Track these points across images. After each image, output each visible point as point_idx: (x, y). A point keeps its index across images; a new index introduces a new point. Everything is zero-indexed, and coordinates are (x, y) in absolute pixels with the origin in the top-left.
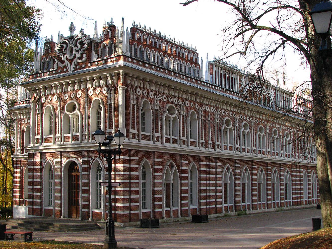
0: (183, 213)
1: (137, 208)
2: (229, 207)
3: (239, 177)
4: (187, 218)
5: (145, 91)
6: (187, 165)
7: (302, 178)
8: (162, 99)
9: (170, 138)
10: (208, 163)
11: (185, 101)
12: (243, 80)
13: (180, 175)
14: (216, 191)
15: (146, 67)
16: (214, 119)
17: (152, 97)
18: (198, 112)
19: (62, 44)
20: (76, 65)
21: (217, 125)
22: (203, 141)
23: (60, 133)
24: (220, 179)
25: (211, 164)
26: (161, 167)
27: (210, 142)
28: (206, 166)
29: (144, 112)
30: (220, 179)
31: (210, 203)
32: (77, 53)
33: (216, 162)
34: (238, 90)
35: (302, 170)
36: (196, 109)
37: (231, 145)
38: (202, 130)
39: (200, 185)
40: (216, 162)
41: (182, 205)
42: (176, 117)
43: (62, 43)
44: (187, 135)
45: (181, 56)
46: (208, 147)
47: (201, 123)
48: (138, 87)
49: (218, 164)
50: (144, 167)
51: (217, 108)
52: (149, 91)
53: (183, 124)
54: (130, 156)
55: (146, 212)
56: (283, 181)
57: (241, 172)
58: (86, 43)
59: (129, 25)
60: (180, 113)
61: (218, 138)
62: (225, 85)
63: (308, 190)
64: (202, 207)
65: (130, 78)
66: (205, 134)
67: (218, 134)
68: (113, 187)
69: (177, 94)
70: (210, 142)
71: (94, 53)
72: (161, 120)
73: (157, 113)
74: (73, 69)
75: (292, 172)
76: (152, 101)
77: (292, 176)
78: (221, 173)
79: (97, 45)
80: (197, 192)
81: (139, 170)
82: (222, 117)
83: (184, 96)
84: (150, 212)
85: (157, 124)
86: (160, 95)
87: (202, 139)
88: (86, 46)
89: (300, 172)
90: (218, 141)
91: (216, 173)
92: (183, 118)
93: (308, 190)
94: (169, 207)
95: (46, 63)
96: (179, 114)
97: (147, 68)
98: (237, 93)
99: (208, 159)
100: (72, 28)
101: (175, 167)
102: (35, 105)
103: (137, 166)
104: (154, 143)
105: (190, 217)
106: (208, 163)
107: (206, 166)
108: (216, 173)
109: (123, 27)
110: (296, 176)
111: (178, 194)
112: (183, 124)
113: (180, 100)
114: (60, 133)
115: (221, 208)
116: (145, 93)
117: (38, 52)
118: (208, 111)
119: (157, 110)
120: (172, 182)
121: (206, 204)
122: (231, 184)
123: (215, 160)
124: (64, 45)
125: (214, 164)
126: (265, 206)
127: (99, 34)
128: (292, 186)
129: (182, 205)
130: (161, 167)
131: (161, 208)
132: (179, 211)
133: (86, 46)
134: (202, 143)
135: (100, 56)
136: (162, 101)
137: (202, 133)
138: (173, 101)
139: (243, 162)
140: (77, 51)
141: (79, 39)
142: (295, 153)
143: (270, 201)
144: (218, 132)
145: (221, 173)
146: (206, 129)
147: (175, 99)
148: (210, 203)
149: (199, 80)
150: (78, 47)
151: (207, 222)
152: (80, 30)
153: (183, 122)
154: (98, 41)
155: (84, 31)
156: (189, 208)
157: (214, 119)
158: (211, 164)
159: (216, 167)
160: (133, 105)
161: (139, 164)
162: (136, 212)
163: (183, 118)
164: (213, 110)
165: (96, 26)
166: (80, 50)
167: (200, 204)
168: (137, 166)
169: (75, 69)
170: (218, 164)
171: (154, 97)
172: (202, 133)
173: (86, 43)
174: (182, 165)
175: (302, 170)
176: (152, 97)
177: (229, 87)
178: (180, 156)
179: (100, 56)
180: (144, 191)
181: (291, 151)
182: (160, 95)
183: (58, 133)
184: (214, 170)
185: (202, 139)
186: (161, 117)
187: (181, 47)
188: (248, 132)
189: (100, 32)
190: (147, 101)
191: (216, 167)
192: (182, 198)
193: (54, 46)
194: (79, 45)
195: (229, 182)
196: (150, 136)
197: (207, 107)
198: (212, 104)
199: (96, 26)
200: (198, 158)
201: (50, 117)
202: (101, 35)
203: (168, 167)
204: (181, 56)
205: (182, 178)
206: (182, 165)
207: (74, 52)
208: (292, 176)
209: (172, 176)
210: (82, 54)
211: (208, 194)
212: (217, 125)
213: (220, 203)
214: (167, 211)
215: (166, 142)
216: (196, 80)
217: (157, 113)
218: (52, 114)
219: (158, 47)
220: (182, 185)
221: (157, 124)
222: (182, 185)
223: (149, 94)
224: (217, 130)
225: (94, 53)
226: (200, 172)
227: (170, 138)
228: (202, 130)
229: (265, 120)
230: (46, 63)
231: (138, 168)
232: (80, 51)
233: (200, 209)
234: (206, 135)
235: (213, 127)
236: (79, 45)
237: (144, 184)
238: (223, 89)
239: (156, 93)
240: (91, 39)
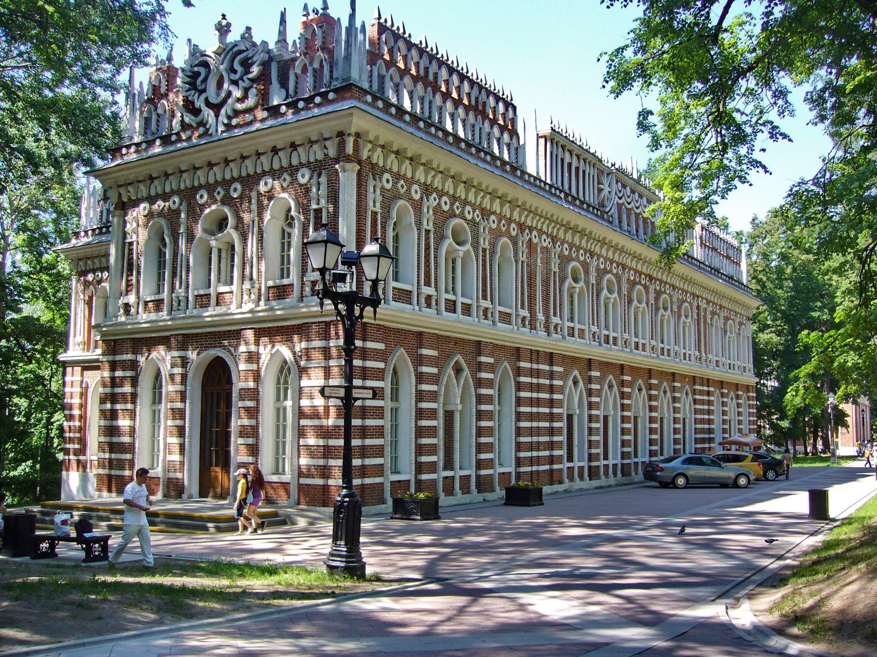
0: (484, 484)
1: (379, 470)
2: (576, 470)
3: (598, 400)
4: (489, 496)
5: (402, 182)
6: (491, 368)
7: (712, 408)
8: (439, 204)
9: (455, 302)
10: (535, 366)
11: (489, 216)
12: (605, 180)
13: (476, 391)
14: (552, 431)
15: (405, 121)
16: (547, 263)
17: (417, 197)
18: (515, 244)
19: (196, 69)
20: (229, 118)
21: (555, 277)
22: (525, 313)
23: (183, 287)
24: (560, 404)
25: (542, 367)
26: (434, 370)
27: (541, 317)
28: (532, 373)
29: (397, 235)
30: (560, 404)
31: (538, 461)
32: (232, 88)
33: (551, 365)
34: (596, 202)
35: (712, 389)
36: (511, 238)
37: (583, 327)
38: (522, 287)
39: (519, 416)
40: (551, 364)
41: (480, 464)
42: (468, 251)
43: (196, 65)
44: (491, 296)
45: (480, 108)
46: (535, 328)
47: (522, 272)
48: (384, 170)
49: (556, 368)
50: (395, 371)
51: (554, 239)
52: (410, 182)
53: (484, 270)
54: (551, 365)
55: (399, 482)
56: (679, 413)
57: (602, 389)
58: (258, 63)
59: (366, 16)
60: (478, 243)
61: (555, 308)
62: (570, 188)
63: (723, 433)
64: (523, 469)
65: (369, 146)
66: (530, 297)
67: (555, 301)
68: (356, 399)
69: (471, 197)
70: (541, 317)
71: (275, 85)
72: (436, 257)
73: (427, 239)
74: (221, 128)
75: (694, 392)
76: (418, 207)
77: (695, 401)
78: (561, 390)
79: (285, 67)
80: (511, 434)
81: (386, 375)
82: (565, 260)
83: (486, 203)
84: (409, 481)
85: (427, 266)
86: (434, 195)
87: (523, 307)
88: (255, 70)
89: (708, 393)
90: (555, 315)
91: (551, 389)
92: (484, 256)
93: (723, 433)
94: (452, 469)
95: (154, 117)
96: (475, 245)
97: (408, 123)
98: (594, 208)
99: (535, 355)
100: (223, 29)
101: (466, 372)
102: (121, 222)
103: (381, 365)
104: (420, 310)
105: (500, 493)
106: (535, 366)
107: (532, 373)
108: (551, 389)
109: (352, 17)
110: (702, 402)
111: (470, 437)
112: (484, 270)
113: (477, 212)
114: (183, 287)
115: (561, 470)
116: (402, 187)
117: (134, 94)
118: (536, 244)
119: (428, 232)
120: (460, 407)
121: (532, 461)
122: (580, 417)
123: (551, 358)
124: (202, 70)
125: (547, 368)
126: (469, 487)
127: (290, 41)
128: (695, 423)
129: (480, 464)
130: (434, 370)
131: (434, 471)
132: (513, 474)
133: (255, 70)
134: (524, 318)
135: (291, 92)
136: (437, 209)
137: (523, 294)
138: (463, 212)
139: (606, 366)
140: (235, 83)
141: (241, 52)
142: (699, 351)
143: (656, 455)
144: (555, 294)
145: (561, 390)
146: (531, 285)
147: (468, 208)
148: (538, 461)
149: (516, 169)
150: (235, 72)
151: (542, 504)
152: (243, 30)
153: (484, 266)
154: (287, 57)
155: (254, 33)
156: (495, 472)
157: (547, 263)
158: (542, 367)
159: (551, 375)
160: (375, 214)
161: (385, 361)
162: (378, 480)
163: (484, 256)
164: (546, 243)
165: (283, 21)
166: (241, 79)
167: (519, 462)
168: (381, 365)
169: (229, 127)
170: (556, 368)
171: (422, 198)
172: (523, 294)
173: (258, 63)
174: (480, 367)
175: (712, 389)
176: (417, 197)
177: (578, 193)
178: (478, 347)
179: (291, 92)
180: (395, 427)
181: (693, 348)
182: (434, 195)
183: (180, 288)
184: (547, 382)
185: (523, 307)
186: (436, 249)
187: (481, 87)
188: (615, 298)
189: (294, 33)
190: (406, 207)
191: (551, 375)
192: (480, 448)
193: (175, 77)
194: (237, 66)
195: (578, 411)
196: (410, 292)
197: (535, 233)
198: (545, 229)
199: (283, 21)
200: (517, 353)
201: (160, 250)
202: (295, 41)
203: (450, 371)
204: (480, 108)
205: (480, 399)
206: (480, 367)
207: (226, 86)
208: (695, 401)
209: (458, 392)
210: (246, 90)
211: (535, 439)
212: (555, 277)
213: (559, 459)
214: (446, 477)
215: (447, 310)
216: (512, 166)
217: (427, 239)
218: (166, 243)
219: (431, 77)
220: (480, 415)
221: (427, 266)
222: (480, 415)
223: (409, 189)
224: (555, 289)
225: (275, 85)
226: (519, 387)
227: (455, 302)
228: (522, 287)
229: (646, 275)
230: (154, 117)
231: (384, 370)
232: (240, 82)
233: (519, 475)
234: (532, 298)
235: (546, 283)
236: (237, 66)
237: (395, 411)
238: (567, 195)
239: (427, 190)
240: (269, 52)
